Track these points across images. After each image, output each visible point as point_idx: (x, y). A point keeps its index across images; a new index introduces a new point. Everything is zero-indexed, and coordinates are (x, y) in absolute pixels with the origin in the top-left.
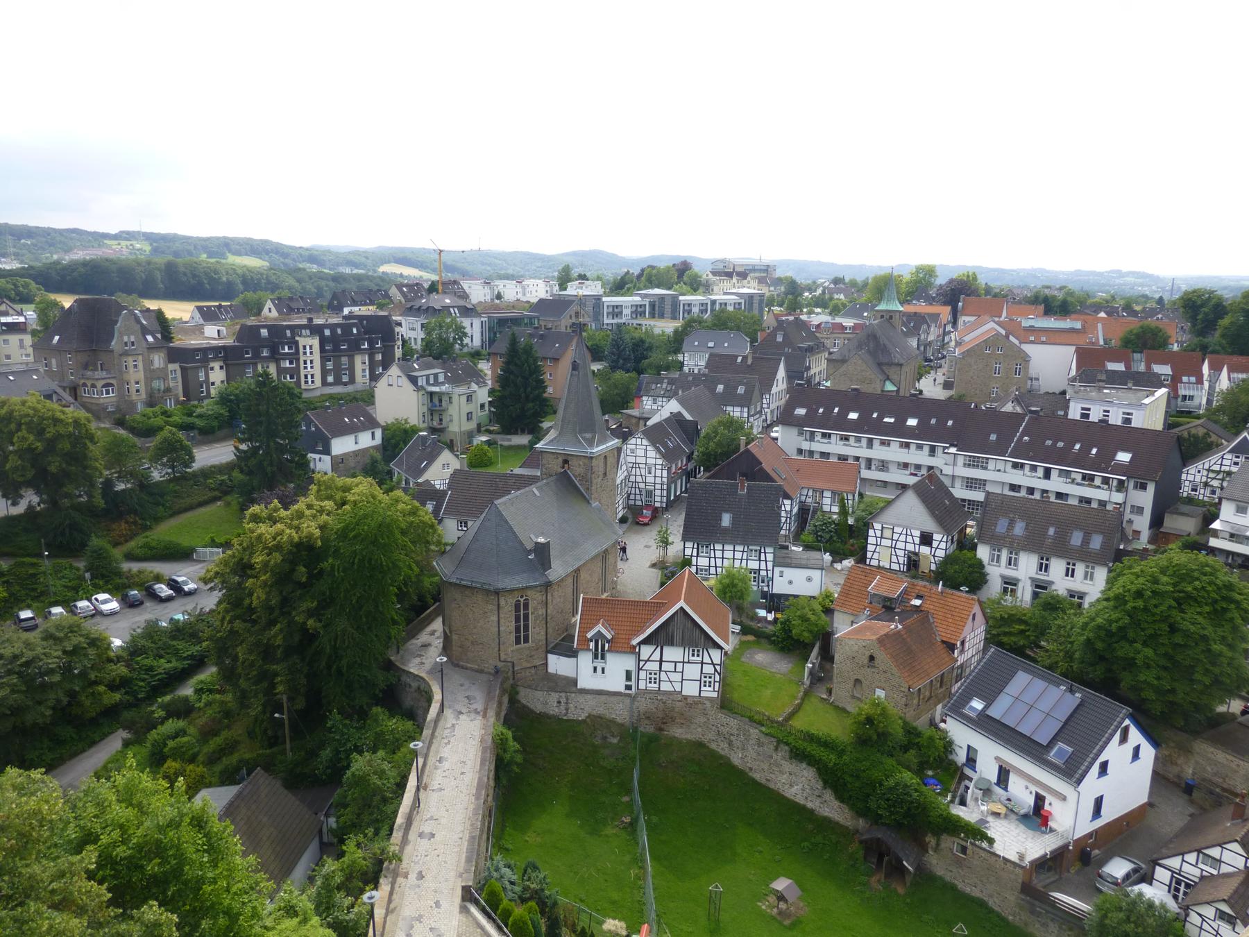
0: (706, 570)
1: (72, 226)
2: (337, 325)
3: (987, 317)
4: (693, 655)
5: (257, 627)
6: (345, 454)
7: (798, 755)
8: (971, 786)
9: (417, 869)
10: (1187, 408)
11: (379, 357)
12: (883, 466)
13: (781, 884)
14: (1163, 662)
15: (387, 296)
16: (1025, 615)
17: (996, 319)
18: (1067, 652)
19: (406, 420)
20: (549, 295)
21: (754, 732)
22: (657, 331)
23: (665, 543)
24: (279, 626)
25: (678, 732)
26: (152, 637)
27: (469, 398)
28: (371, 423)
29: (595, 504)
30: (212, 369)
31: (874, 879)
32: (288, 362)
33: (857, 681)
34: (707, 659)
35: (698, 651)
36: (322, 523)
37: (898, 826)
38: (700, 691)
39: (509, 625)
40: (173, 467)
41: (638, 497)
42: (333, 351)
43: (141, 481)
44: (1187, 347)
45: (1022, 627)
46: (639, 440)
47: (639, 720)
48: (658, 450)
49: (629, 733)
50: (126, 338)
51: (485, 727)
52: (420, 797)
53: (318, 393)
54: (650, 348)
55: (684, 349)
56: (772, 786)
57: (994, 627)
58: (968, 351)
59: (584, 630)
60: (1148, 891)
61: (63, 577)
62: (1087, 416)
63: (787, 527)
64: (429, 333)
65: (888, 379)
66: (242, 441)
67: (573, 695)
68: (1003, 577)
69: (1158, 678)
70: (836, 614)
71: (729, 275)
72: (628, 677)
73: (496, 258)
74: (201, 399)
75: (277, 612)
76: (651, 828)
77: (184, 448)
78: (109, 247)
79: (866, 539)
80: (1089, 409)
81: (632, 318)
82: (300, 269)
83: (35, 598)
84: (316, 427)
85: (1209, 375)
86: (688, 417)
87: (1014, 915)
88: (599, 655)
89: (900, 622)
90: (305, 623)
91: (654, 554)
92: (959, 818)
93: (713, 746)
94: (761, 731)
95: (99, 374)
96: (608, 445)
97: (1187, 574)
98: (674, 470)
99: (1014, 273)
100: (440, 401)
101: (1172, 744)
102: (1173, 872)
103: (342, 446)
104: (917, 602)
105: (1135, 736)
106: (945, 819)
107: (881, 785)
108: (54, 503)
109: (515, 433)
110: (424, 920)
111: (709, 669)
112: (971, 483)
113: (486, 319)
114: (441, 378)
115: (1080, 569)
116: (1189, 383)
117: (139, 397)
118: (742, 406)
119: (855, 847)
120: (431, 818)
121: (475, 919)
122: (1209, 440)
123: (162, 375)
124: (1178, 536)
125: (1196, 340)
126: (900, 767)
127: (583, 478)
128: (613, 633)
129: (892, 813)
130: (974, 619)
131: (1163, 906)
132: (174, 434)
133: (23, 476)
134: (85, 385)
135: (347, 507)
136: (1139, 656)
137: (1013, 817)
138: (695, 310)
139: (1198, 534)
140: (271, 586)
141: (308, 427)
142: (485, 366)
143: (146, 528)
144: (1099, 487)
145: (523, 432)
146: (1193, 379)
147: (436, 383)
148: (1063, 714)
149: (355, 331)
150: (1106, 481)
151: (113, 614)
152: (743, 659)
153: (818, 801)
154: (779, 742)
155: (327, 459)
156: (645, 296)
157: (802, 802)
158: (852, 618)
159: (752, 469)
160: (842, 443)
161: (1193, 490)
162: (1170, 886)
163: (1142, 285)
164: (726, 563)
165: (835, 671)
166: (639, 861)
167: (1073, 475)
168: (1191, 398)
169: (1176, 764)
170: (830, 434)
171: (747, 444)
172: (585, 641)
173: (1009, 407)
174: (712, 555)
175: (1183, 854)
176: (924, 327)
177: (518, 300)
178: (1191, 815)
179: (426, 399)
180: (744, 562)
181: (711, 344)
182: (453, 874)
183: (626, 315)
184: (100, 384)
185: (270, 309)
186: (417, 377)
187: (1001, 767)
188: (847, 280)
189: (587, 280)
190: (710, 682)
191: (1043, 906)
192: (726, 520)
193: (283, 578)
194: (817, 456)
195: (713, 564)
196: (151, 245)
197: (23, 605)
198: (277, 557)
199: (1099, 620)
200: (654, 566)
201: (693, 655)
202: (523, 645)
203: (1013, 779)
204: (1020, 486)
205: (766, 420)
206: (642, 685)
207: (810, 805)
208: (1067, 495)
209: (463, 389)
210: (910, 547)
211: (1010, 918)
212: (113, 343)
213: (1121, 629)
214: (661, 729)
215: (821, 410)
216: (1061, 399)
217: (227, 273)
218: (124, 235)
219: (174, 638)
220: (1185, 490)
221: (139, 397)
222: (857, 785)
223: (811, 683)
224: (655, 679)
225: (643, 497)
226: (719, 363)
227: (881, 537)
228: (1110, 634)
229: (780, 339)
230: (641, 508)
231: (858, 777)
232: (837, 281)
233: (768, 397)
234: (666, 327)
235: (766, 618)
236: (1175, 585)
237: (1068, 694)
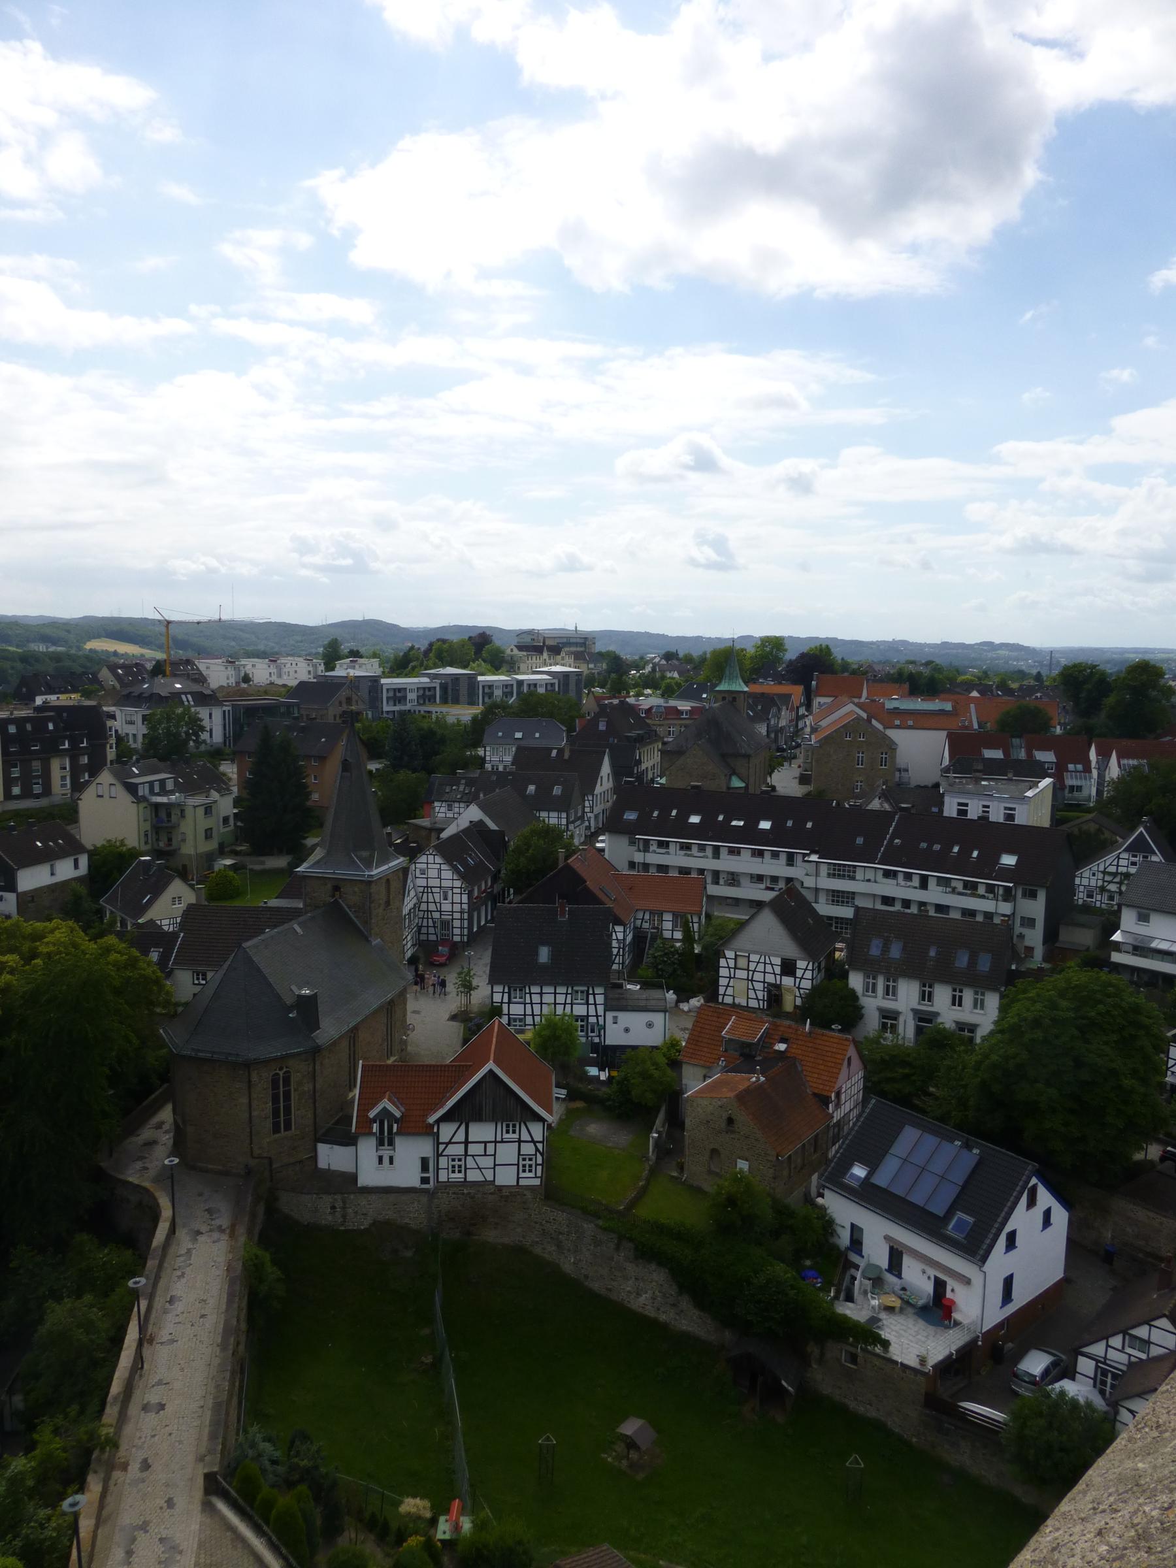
0: (520, 1020)
2: (26, 719)
3: (845, 699)
4: (508, 1132)
6: (36, 890)
7: (646, 1254)
8: (859, 1275)
9: (140, 1455)
11: (85, 760)
12: (733, 879)
13: (630, 1427)
15: (95, 680)
17: (856, 700)
20: (311, 676)
21: (589, 1227)
22: (451, 720)
25: (490, 1235)
27: (208, 810)
28: (73, 848)
29: (376, 942)
33: (714, 1152)
38: (518, 1178)
41: (431, 930)
45: (907, 1071)
46: (431, 858)
55: (486, 739)
64: (153, 728)
65: (734, 773)
67: (352, 1197)
71: (538, 650)
73: (241, 630)
81: (419, 704)
86: (492, 826)
88: (385, 1140)
93: (538, 1250)
94: (597, 1225)
96: (391, 864)
98: (476, 894)
100: (169, 815)
102: (1097, 1361)
104: (782, 1047)
105: (1045, 1198)
109: (270, 854)
112: (838, 897)
113: (230, 708)
114: (170, 785)
115: (968, 996)
118: (559, 811)
120: (160, 1383)
121: (223, 1519)
122: (1102, 837)
128: (403, 1109)
131: (1089, 1404)
137: (910, 1310)
138: (498, 693)
142: (229, 769)
144: (983, 897)
146: (1080, 767)
147: (164, 792)
148: (959, 1176)
149: (51, 726)
156: (436, 676)
157: (653, 1314)
158: (704, 1071)
162: (1095, 1379)
163: (1018, 660)
164: (546, 1010)
167: (954, 884)
168: (1079, 788)
171: (567, 858)
172: (365, 1125)
173: (876, 804)
174: (528, 1000)
175: (1107, 1338)
176: (774, 710)
177: (272, 683)
180: (568, 1007)
181: (519, 735)
187: (892, 1249)
188: (681, 655)
189: (361, 657)
190: (530, 1166)
194: (653, 871)
195: (529, 1011)
199: (994, 1057)
200: (453, 1018)
201: (508, 1132)
202: (283, 1134)
203: (907, 1262)
204: (894, 899)
205: (588, 828)
206: (443, 1177)
207: (663, 1317)
209: (199, 800)
210: (770, 979)
211: (914, 1440)
215: (656, 814)
216: (932, 793)
220: (1081, 897)
223: (658, 1158)
224: (460, 1166)
225: (438, 930)
226: (524, 756)
227: (735, 968)
229: (602, 726)
230: (436, 944)
232: (669, 656)
233: (590, 798)
234: (463, 714)
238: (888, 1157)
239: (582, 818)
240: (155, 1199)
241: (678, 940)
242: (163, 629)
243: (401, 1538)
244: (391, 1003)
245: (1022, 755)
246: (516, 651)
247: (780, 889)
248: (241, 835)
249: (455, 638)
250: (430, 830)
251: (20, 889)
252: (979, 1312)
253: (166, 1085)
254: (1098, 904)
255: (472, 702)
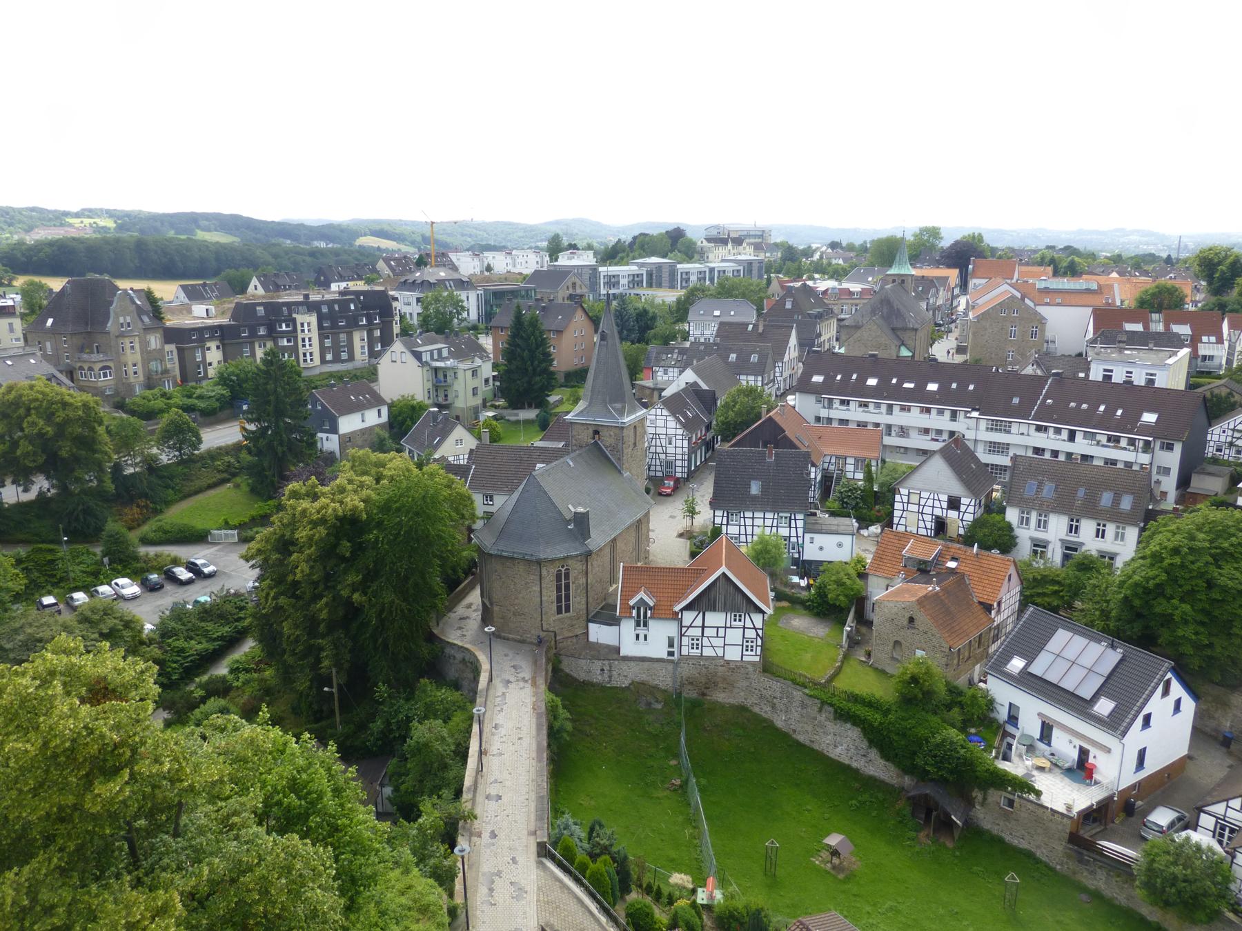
0: (736, 538)
1: (31, 205)
2: (334, 301)
3: (999, 280)
4: (735, 620)
5: (301, 603)
6: (352, 433)
7: (843, 716)
8: (1015, 743)
9: (489, 828)
10: (1207, 368)
11: (377, 333)
12: (903, 432)
13: (834, 840)
14: (1200, 617)
15: (375, 270)
16: (1058, 576)
17: (1009, 281)
18: (1103, 611)
19: (413, 396)
21: (798, 694)
22: (658, 301)
23: (692, 512)
24: (325, 600)
25: (721, 697)
26: (180, 619)
27: (474, 373)
28: (377, 401)
29: (626, 474)
30: (209, 349)
31: (922, 834)
32: (285, 340)
33: (897, 643)
34: (749, 624)
35: (740, 616)
36: (364, 497)
37: (942, 782)
39: (550, 594)
40: (180, 450)
41: (659, 468)
42: (332, 328)
43: (149, 465)
44: (1204, 306)
45: (1056, 588)
46: (659, 411)
47: (682, 685)
48: (677, 419)
49: (673, 699)
50: (121, 320)
51: (536, 694)
52: (484, 762)
53: (317, 371)
54: (654, 318)
55: (690, 317)
56: (816, 747)
57: (1028, 588)
58: (982, 314)
59: (625, 599)
60: (1195, 837)
61: (81, 563)
62: (1110, 377)
63: (814, 494)
64: (426, 308)
65: (903, 344)
66: (250, 421)
68: (1032, 539)
69: (1196, 633)
70: (870, 577)
71: (723, 242)
72: (671, 645)
73: (476, 229)
74: (199, 380)
75: (321, 587)
76: (702, 790)
77: (190, 430)
78: (71, 225)
79: (892, 506)
80: (1111, 371)
82: (274, 245)
83: (55, 585)
84: (322, 405)
85: (1229, 335)
86: (704, 386)
87: (1062, 864)
88: (641, 622)
89: (938, 584)
90: (350, 597)
91: (682, 523)
92: (1006, 773)
93: (756, 710)
94: (804, 693)
95: (95, 357)
97: (1224, 531)
98: (694, 440)
99: (1015, 234)
100: (445, 376)
101: (1210, 699)
102: (1217, 818)
103: (349, 424)
104: (952, 564)
105: (1177, 689)
106: (992, 773)
107: (927, 742)
108: (64, 489)
109: (522, 408)
110: (504, 875)
111: (751, 634)
112: (994, 447)
114: (445, 353)
115: (1111, 529)
116: (1209, 343)
117: (137, 382)
118: (755, 375)
119: (901, 804)
120: (496, 781)
121: (552, 873)
122: (1232, 400)
123: (159, 356)
124: (1206, 496)
125: (1213, 299)
126: (945, 725)
127: (614, 448)
129: (939, 769)
130: (1009, 580)
131: (1210, 849)
132: (180, 416)
133: (34, 461)
134: (81, 368)
135: (385, 482)
136: (1178, 612)
137: (1057, 770)
138: (693, 278)
139: (1225, 494)
140: (315, 561)
141: (314, 405)
142: (487, 342)
143: (157, 512)
144: (1125, 449)
145: (530, 406)
146: (1213, 339)
147: (441, 358)
148: (1106, 668)
149: (352, 307)
150: (1132, 442)
151: (134, 598)
152: (780, 625)
153: (864, 760)
154: (823, 703)
155: (335, 438)
156: (643, 265)
157: (847, 762)
158: (887, 582)
159: (774, 435)
160: (861, 409)
161: (1217, 450)
162: (1214, 832)
163: (1148, 244)
164: (757, 531)
165: (875, 634)
166: (692, 821)
167: (1098, 437)
168: (1211, 358)
169: (1213, 718)
170: (848, 401)
171: (769, 411)
172: (627, 609)
173: (1029, 370)
174: (742, 523)
175: (1227, 800)
176: (933, 291)
178: (1230, 767)
179: (430, 375)
180: (774, 529)
181: (717, 313)
182: (525, 832)
183: (623, 285)
184: (97, 367)
185: (256, 287)
186: (421, 353)
187: (1043, 723)
188: (844, 244)
189: (578, 249)
191: (1092, 855)
192: (755, 488)
193: (328, 552)
194: (835, 424)
195: (743, 532)
196: (115, 222)
197: (44, 591)
198: (322, 531)
199: (1137, 578)
200: (681, 535)
201: (735, 620)
202: (564, 615)
203: (1056, 733)
204: (1043, 450)
205: (779, 389)
206: (685, 651)
207: (855, 765)
208: (1092, 457)
209: (466, 365)
210: (938, 512)
211: (1058, 867)
212: (109, 325)
213: (1158, 585)
214: (704, 694)
215: (839, 377)
216: (1081, 360)
217: (200, 250)
218: (87, 213)
219: (202, 620)
220: (1210, 450)
221: (137, 382)
222: (903, 743)
223: (849, 646)
225: (664, 468)
226: (727, 330)
227: (908, 503)
228: (1147, 591)
229: (789, 306)
230: (662, 479)
231: (904, 735)
232: (834, 245)
233: (780, 365)
234: (668, 297)
235: (798, 585)
236: (1211, 541)
237: (1110, 651)
238: (1043, 653)
239: (773, 381)
240: (475, 656)
241: (860, 480)
242: (429, 226)
243: (671, 901)
244: (639, 521)
245: (1160, 328)
246: (705, 243)
247: (944, 441)
248: (501, 392)
249: (654, 232)
250: (654, 389)
251: (341, 433)
252: (1117, 774)
253: (471, 578)
254: (1226, 457)
255: (672, 286)
